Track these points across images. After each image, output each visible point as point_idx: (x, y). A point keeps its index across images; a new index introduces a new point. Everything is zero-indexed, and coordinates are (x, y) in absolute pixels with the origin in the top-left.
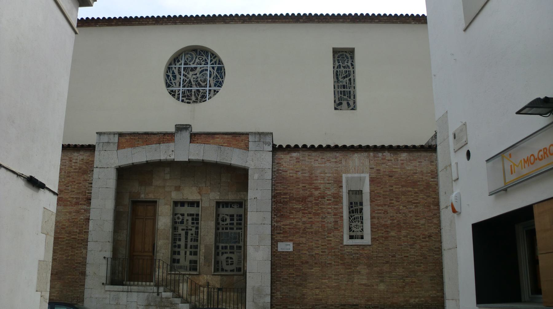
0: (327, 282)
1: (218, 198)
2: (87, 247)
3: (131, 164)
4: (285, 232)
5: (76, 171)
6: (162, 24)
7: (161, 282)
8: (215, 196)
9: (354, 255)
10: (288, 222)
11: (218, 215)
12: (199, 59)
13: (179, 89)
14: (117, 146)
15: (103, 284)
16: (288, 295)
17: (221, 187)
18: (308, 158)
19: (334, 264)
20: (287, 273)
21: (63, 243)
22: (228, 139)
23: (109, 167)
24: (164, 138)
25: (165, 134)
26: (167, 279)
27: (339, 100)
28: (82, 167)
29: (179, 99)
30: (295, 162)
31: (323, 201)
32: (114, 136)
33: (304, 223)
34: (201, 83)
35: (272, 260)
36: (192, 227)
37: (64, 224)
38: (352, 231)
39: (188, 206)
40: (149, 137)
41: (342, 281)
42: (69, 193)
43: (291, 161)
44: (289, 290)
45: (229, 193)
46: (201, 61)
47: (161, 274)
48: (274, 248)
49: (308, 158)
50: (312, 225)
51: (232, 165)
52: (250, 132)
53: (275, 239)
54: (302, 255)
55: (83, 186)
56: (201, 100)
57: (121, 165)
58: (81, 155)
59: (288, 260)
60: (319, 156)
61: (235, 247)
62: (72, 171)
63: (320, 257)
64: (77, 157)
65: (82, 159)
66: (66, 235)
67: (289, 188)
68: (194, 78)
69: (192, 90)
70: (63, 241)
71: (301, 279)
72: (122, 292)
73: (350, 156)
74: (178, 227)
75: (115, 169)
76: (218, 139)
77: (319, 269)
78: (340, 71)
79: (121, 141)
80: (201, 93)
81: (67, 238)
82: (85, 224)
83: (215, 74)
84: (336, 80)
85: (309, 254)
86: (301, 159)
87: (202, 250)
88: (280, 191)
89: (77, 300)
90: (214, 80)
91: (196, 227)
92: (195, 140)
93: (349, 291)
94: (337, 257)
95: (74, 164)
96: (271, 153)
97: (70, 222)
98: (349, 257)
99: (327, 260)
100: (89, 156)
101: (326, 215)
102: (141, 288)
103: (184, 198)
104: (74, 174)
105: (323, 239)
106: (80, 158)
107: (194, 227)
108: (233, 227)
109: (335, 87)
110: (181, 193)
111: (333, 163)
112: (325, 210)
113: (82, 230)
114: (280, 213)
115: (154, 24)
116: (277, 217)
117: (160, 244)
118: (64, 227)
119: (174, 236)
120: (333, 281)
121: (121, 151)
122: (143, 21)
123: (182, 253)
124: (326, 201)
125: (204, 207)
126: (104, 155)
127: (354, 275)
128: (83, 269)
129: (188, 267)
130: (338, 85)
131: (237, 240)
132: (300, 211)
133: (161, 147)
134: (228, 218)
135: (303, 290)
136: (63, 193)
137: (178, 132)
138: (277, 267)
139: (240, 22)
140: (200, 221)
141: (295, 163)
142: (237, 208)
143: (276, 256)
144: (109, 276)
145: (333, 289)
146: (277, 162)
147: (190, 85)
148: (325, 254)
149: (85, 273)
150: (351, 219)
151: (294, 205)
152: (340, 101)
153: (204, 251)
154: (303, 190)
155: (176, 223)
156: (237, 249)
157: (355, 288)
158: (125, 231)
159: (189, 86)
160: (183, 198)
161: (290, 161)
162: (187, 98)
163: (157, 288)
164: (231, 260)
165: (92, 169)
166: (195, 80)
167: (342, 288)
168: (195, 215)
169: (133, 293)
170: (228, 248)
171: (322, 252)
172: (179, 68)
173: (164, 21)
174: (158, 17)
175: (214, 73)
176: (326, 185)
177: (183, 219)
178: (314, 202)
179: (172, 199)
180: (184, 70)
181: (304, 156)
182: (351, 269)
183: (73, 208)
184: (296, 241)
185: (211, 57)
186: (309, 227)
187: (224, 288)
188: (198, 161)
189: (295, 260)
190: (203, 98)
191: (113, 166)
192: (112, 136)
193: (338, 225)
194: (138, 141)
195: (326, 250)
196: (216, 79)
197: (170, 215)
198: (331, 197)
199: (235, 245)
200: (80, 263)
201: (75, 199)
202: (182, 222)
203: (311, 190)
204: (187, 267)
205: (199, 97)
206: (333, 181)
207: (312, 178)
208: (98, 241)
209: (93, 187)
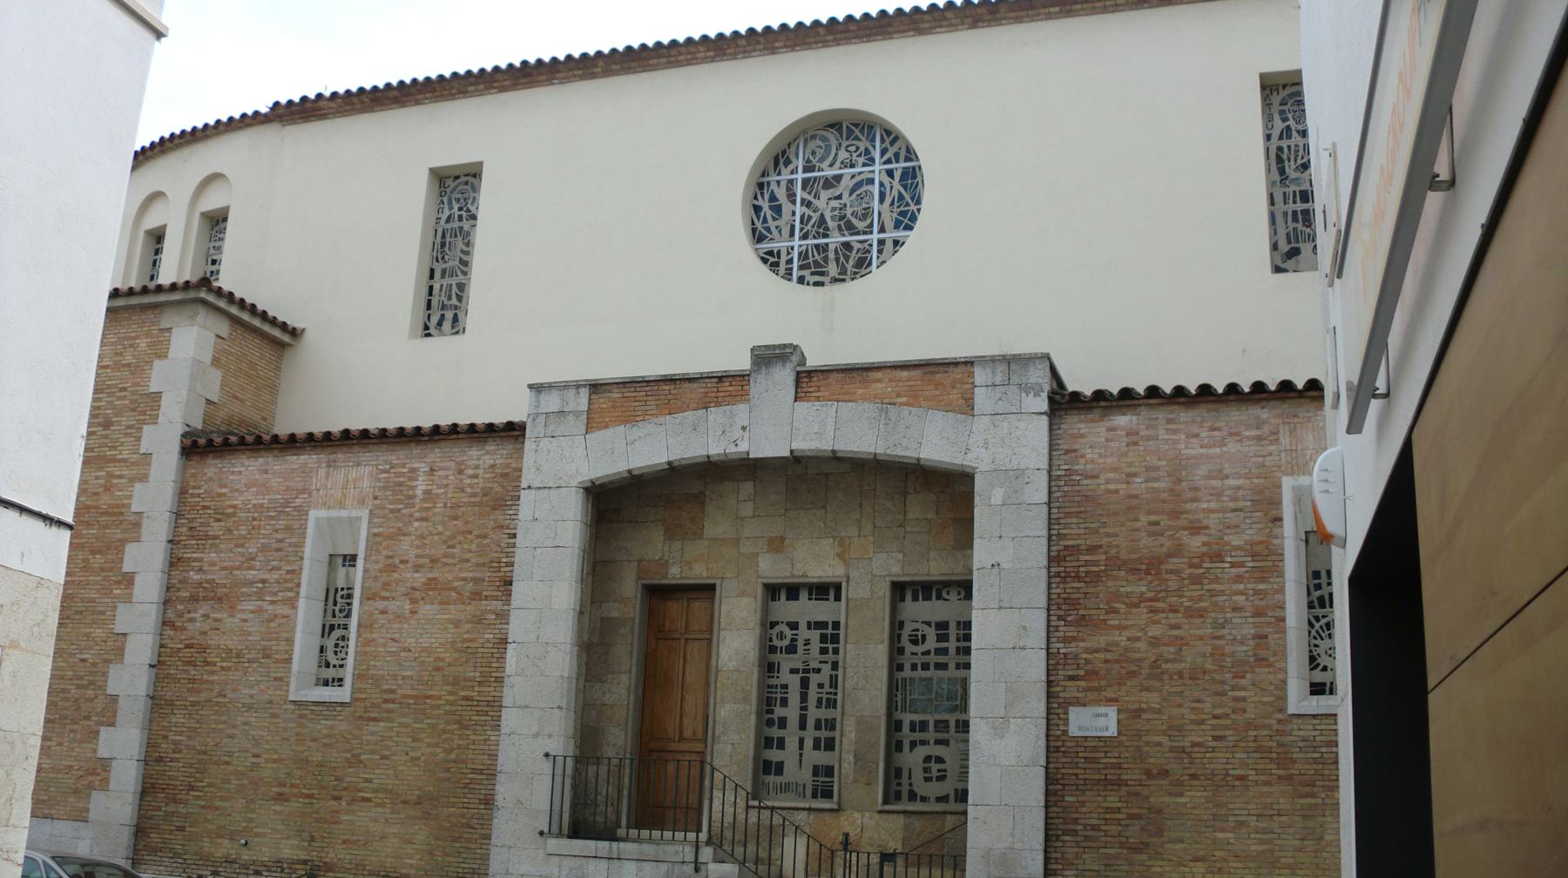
0: (1231, 841)
1: (896, 569)
3: (626, 475)
4: (1092, 674)
5: (474, 502)
6: (734, 57)
8: (891, 564)
9: (1324, 750)
10: (1101, 640)
11: (897, 626)
12: (847, 151)
13: (791, 244)
14: (585, 422)
15: (541, 833)
19: (1256, 778)
20: (1099, 807)
21: (436, 712)
22: (912, 383)
25: (721, 378)
27: (1289, 242)
29: (791, 274)
30: (1124, 444)
31: (1218, 571)
32: (578, 393)
33: (1155, 642)
34: (854, 221)
35: (1051, 766)
36: (821, 662)
37: (442, 655)
38: (1321, 667)
39: (810, 599)
41: (1282, 836)
43: (1112, 440)
44: (1106, 865)
45: (933, 554)
46: (855, 155)
47: (729, 810)
48: (1058, 725)
50: (1181, 650)
51: (922, 462)
52: (976, 357)
54: (1147, 749)
55: (492, 545)
56: (855, 273)
57: (598, 479)
58: (488, 453)
59: (1102, 766)
61: (952, 725)
63: (1208, 755)
64: (479, 459)
65: (493, 466)
66: (444, 688)
67: (1106, 530)
68: (834, 209)
69: (827, 245)
70: (438, 707)
71: (1143, 829)
73: (1306, 414)
77: (1206, 794)
78: (1289, 147)
79: (597, 406)
80: (854, 252)
81: (447, 697)
82: (498, 655)
83: (895, 193)
84: (1277, 178)
85: (1169, 744)
86: (1144, 433)
87: (848, 735)
91: (833, 663)
92: (811, 390)
93: (1307, 872)
94: (1265, 755)
95: (469, 481)
97: (457, 650)
98: (1309, 755)
99: (1231, 766)
101: (1228, 615)
102: (649, 849)
105: (1217, 694)
106: (488, 462)
109: (1276, 200)
111: (1252, 442)
112: (1225, 598)
114: (1075, 612)
115: (712, 60)
117: (723, 714)
119: (768, 692)
120: (1252, 836)
121: (598, 436)
122: (680, 54)
123: (792, 743)
124: (1226, 570)
127: (1324, 816)
130: (1285, 193)
131: (958, 702)
132: (1142, 605)
133: (711, 418)
134: (931, 634)
138: (1067, 788)
139: (963, 24)
140: (841, 645)
141: (1124, 449)
143: (1063, 752)
145: (1250, 864)
146: (1065, 447)
147: (821, 230)
148: (1225, 743)
150: (1317, 626)
151: (1120, 583)
152: (1293, 245)
153: (853, 735)
154: (1150, 534)
155: (773, 650)
156: (957, 732)
157: (1328, 861)
159: (818, 233)
161: (1109, 444)
164: (941, 766)
166: (836, 213)
167: (1283, 860)
168: (830, 626)
171: (1215, 738)
172: (791, 182)
173: (738, 46)
174: (721, 36)
175: (892, 187)
176: (1227, 515)
177: (794, 640)
178: (1187, 572)
179: (759, 577)
180: (804, 188)
182: (1313, 795)
183: (465, 610)
184: (1128, 702)
185: (883, 141)
186: (1171, 657)
188: (819, 454)
189: (1126, 766)
191: (574, 483)
192: (572, 392)
193: (1268, 649)
195: (1227, 733)
196: (898, 207)
198: (1243, 553)
201: (471, 584)
202: (791, 649)
203: (1178, 535)
205: (849, 266)
206: (1249, 503)
209: (518, 545)
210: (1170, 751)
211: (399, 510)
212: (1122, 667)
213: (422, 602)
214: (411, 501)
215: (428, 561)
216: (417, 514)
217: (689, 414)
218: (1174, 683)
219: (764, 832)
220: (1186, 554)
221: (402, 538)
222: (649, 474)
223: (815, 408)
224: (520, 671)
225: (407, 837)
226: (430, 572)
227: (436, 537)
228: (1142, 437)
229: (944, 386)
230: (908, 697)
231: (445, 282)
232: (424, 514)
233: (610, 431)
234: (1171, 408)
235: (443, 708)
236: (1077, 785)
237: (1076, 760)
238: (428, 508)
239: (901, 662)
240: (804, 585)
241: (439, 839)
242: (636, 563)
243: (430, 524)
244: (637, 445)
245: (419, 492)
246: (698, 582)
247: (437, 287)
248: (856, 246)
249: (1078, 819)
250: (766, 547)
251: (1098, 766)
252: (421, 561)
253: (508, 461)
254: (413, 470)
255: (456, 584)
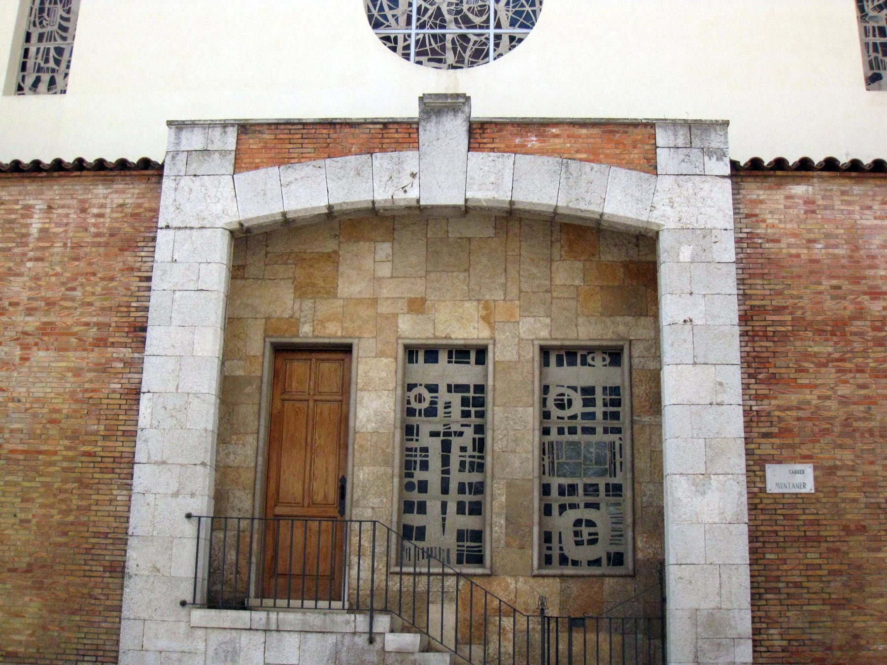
1: (544, 333)
2: (129, 481)
4: (785, 431)
7: (369, 600)
10: (793, 398)
15: (183, 604)
16: (805, 637)
17: (555, 301)
18: (842, 201)
21: (51, 469)
23: (208, 226)
24: (386, 136)
25: (386, 124)
26: (387, 589)
28: (120, 229)
30: (802, 212)
32: (225, 132)
33: (844, 401)
34: (471, 16)
36: (462, 425)
39: (449, 362)
40: (335, 133)
42: (76, 308)
44: (810, 622)
45: (581, 320)
47: (366, 574)
49: (842, 201)
50: (869, 408)
53: (753, 454)
54: (843, 505)
57: (247, 220)
58: (116, 192)
59: (801, 523)
60: (875, 195)
61: (602, 489)
62: (88, 240)
66: (61, 442)
69: (444, 35)
71: (845, 585)
72: (248, 631)
74: (418, 426)
75: (227, 232)
76: (557, 141)
81: (64, 453)
82: (126, 407)
85: (865, 500)
86: (820, 202)
88: (763, 303)
89: (97, 656)
90: (510, 9)
92: (485, 141)
95: (93, 221)
96: (728, 182)
97: (76, 401)
100: (142, 195)
102: (314, 619)
103: (437, 334)
104: (94, 249)
107: (469, 426)
108: (593, 426)
110: (429, 318)
113: (115, 428)
114: (766, 370)
116: (756, 383)
117: (361, 477)
118: (55, 416)
119: (407, 456)
123: (433, 507)
125: (502, 362)
126: (191, 190)
128: (116, 552)
129: (451, 552)
130: (865, 27)
131: (607, 466)
132: (830, 365)
133: (376, 163)
134: (577, 399)
135: (853, 619)
136: (57, 308)
137: (429, 117)
138: (767, 545)
141: (803, 216)
142: (604, 366)
143: (761, 509)
144: (203, 579)
146: (746, 211)
147: (438, 22)
149: (124, 567)
151: (807, 343)
153: (503, 499)
154: (833, 298)
155: (411, 412)
156: (606, 495)
158: (251, 439)
159: (436, 25)
160: (434, 334)
161: (786, 210)
162: (430, 56)
163: (368, 618)
164: (592, 530)
165: (151, 235)
166: (452, 8)
169: (286, 634)
170: (581, 491)
177: (433, 403)
179: (398, 338)
181: (828, 194)
184: (823, 459)
186: (861, 415)
187: (591, 618)
189: (825, 522)
190: (480, 55)
191: (221, 223)
194: (300, 146)
197: (396, 388)
199: (602, 482)
200: (106, 535)
201: (95, 329)
202: (431, 412)
203: (859, 299)
204: (448, 550)
205: (467, 55)
207: (858, 262)
208: (169, 462)
210: (867, 507)
211: (10, 249)
212: (814, 425)
213: (35, 348)
214: (24, 240)
215: (43, 304)
216: (31, 254)
217: (352, 158)
218: (866, 441)
219: (407, 600)
220: (869, 318)
221: (12, 278)
222: (304, 219)
223: (490, 159)
224: (155, 423)
225: (12, 609)
226: (45, 315)
227: (53, 279)
228: (819, 206)
229: (625, 145)
230: (556, 461)
231: (43, 46)
232: (39, 254)
233: (261, 172)
234: (843, 181)
235: (58, 464)
236: (777, 542)
237: (775, 517)
238: (44, 249)
239: (548, 425)
240: (444, 347)
241: (53, 612)
242: (263, 321)
243: (46, 264)
244: (293, 187)
245: (34, 230)
246: (333, 341)
247: (33, 50)
248: (473, 38)
249: (779, 577)
250: (406, 309)
251: (797, 523)
252: (34, 304)
253: (140, 201)
254: (28, 207)
255: (76, 329)
